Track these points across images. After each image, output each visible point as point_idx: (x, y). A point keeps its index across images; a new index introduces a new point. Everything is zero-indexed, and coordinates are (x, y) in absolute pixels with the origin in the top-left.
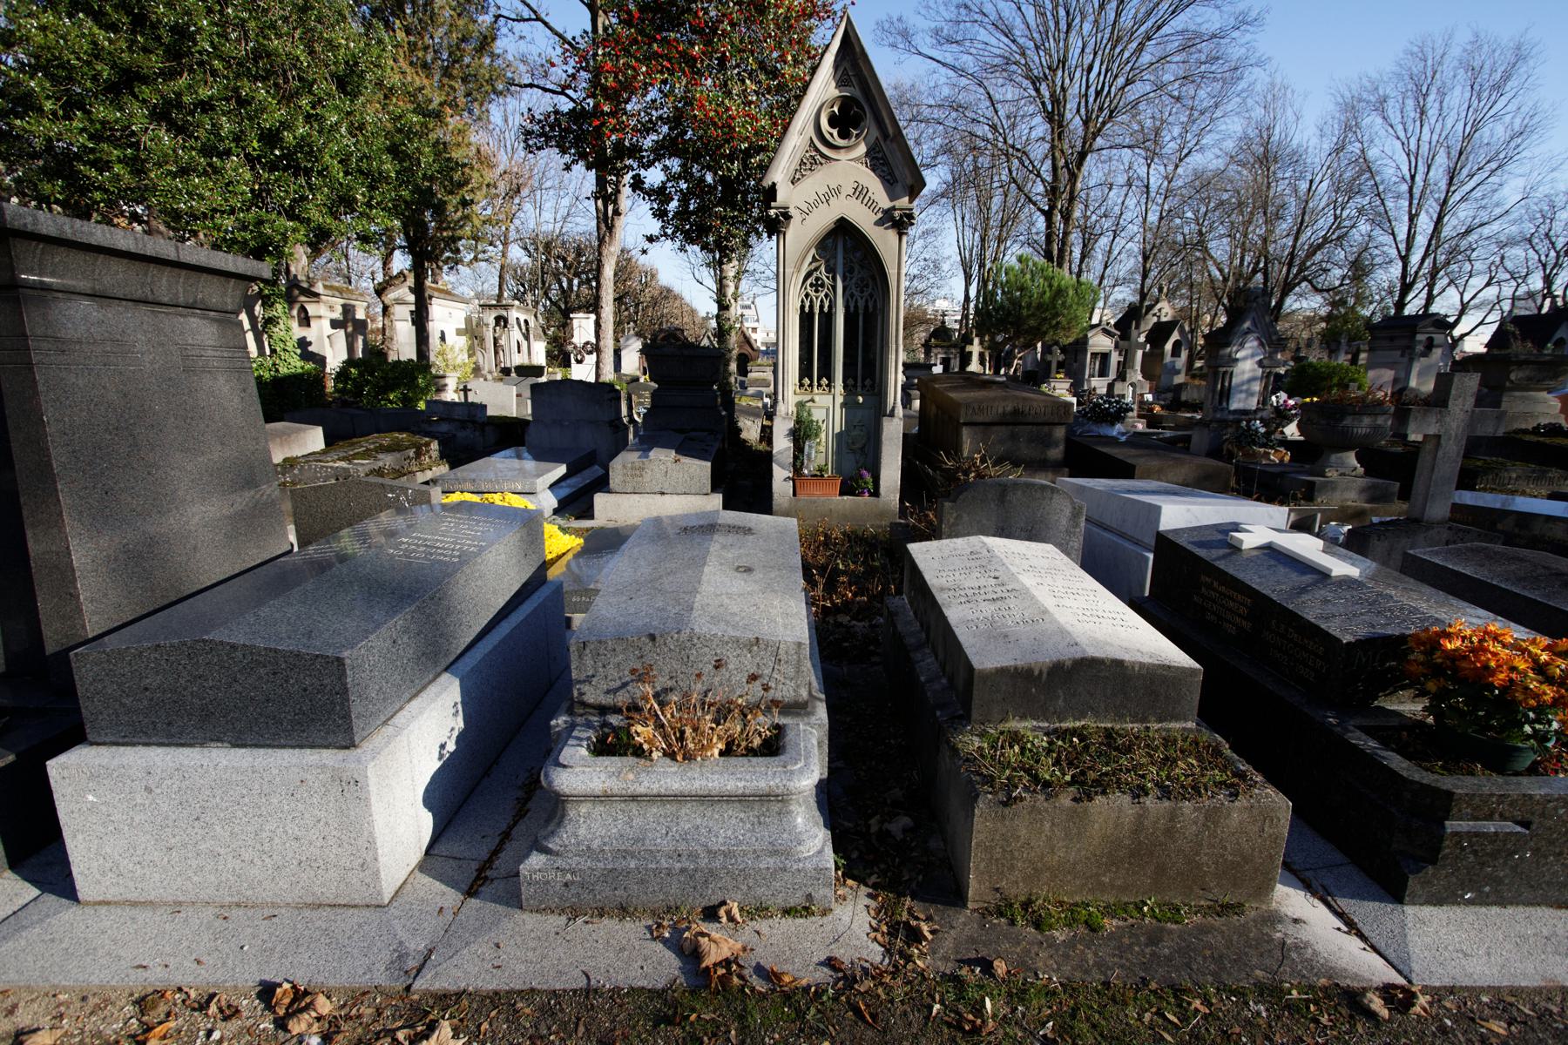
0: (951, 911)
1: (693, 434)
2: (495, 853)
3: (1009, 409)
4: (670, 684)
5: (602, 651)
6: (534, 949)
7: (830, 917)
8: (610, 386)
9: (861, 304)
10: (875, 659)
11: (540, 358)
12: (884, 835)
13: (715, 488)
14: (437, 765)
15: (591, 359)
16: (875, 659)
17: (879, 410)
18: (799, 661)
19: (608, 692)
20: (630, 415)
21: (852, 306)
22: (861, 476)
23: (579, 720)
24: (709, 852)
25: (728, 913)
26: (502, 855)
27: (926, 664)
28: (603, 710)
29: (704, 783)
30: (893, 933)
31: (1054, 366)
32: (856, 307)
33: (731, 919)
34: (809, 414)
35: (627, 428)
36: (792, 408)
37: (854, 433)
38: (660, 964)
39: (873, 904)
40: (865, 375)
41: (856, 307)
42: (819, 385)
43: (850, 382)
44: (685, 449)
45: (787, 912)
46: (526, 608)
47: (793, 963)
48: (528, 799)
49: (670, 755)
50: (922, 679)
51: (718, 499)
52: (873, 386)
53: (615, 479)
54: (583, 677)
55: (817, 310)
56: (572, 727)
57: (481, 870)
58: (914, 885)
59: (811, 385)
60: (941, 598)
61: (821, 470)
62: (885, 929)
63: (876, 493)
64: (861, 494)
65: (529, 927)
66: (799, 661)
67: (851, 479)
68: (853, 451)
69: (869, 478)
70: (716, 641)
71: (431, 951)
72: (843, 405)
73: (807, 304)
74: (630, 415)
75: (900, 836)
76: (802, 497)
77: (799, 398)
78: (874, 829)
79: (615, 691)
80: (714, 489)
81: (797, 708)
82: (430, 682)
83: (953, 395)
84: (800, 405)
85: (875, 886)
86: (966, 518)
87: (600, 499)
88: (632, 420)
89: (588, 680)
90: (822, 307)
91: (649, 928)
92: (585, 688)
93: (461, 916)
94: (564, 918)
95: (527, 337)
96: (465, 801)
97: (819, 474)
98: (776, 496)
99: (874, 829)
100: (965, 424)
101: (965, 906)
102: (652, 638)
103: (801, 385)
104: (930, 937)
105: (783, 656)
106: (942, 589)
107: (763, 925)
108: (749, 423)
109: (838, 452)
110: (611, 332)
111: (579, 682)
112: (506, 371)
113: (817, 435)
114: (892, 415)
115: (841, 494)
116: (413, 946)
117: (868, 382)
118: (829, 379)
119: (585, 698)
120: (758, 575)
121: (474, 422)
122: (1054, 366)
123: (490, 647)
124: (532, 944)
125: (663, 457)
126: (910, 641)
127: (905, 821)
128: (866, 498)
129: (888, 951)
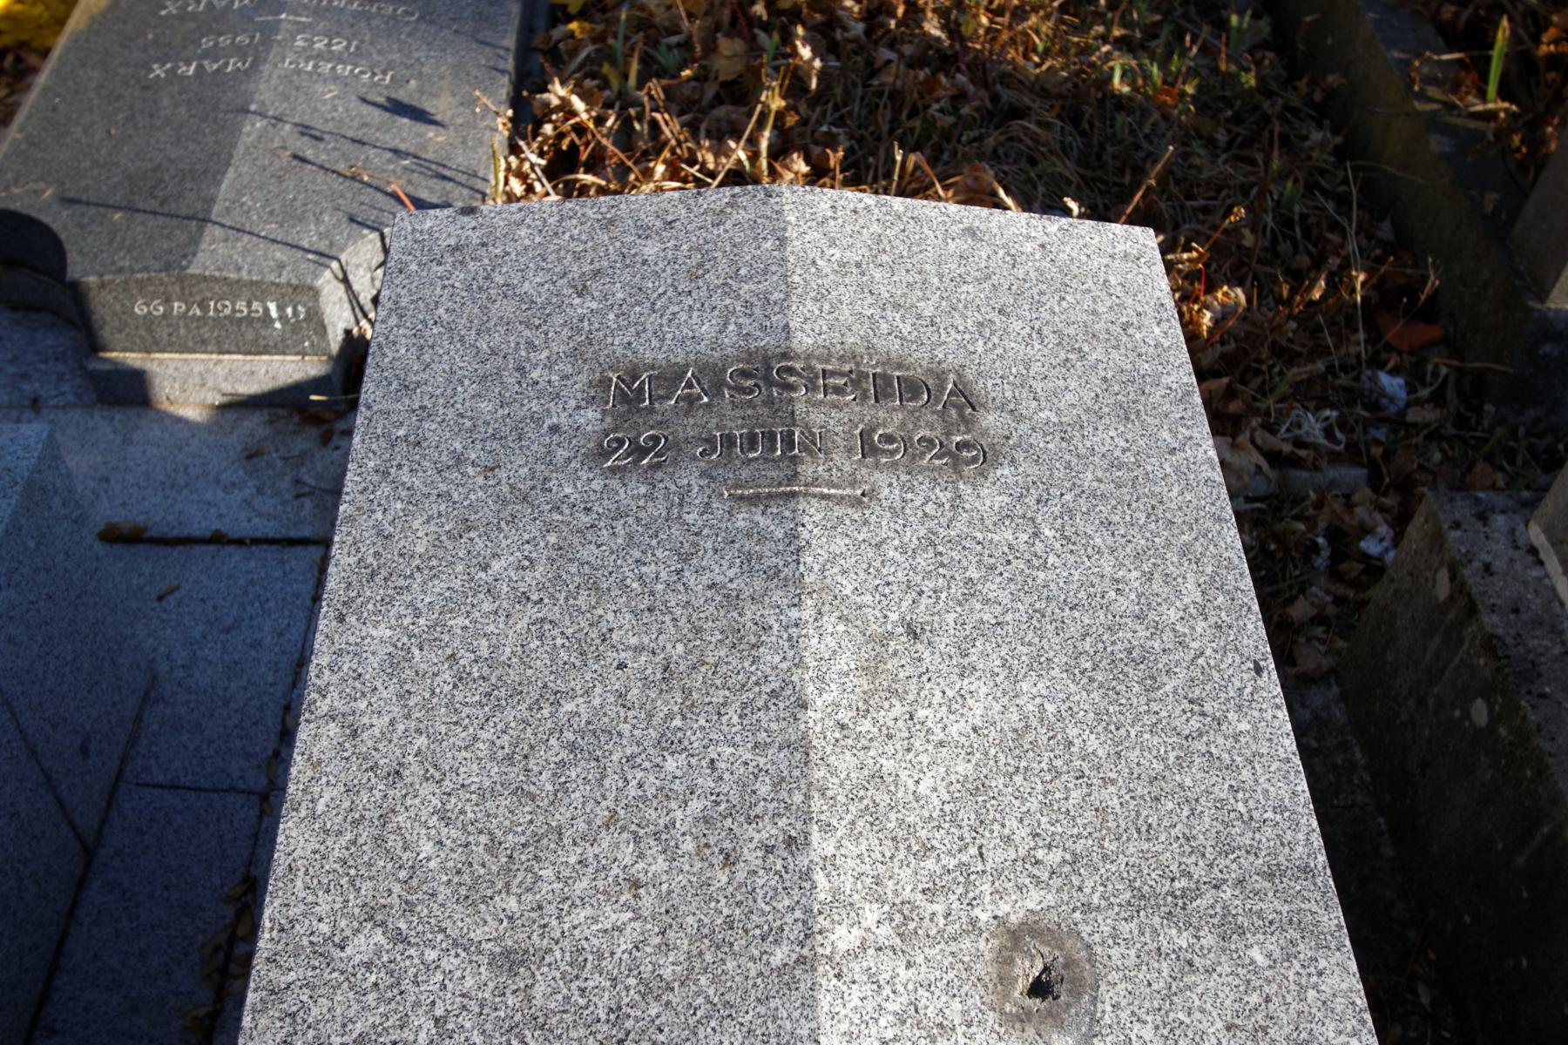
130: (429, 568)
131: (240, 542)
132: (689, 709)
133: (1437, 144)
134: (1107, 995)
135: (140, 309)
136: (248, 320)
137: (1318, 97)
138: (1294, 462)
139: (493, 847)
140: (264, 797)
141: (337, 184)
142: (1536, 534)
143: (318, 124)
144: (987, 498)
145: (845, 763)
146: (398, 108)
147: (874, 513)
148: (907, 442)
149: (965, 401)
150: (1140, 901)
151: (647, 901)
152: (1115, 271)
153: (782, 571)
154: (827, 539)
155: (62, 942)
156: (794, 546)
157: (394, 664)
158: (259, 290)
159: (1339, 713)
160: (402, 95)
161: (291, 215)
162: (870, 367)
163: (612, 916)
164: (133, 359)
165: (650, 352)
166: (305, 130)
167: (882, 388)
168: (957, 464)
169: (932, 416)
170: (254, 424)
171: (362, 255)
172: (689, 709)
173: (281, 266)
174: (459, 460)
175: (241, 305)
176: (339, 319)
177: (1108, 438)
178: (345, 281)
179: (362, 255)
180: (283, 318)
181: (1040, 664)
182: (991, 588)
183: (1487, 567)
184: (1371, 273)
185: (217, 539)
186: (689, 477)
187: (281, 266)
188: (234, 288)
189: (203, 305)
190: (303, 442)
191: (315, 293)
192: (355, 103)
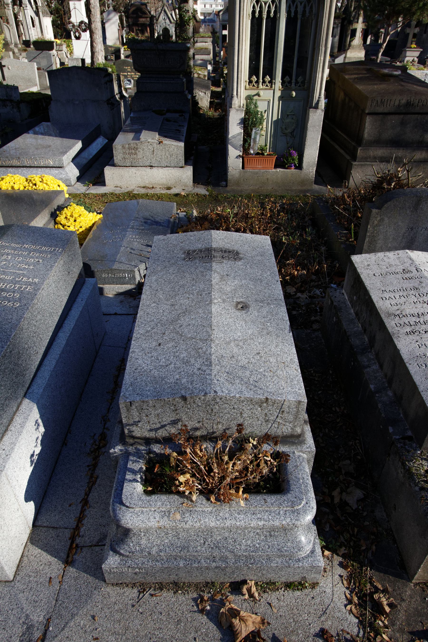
0: (399, 583)
1: (169, 115)
2: (80, 520)
3: (404, 101)
4: (197, 425)
5: (144, 407)
6: (119, 621)
7: (318, 589)
8: (103, 71)
9: (300, 9)
10: (315, 326)
11: (49, 35)
12: (344, 504)
13: (187, 162)
14: (29, 469)
15: (86, 35)
16: (315, 326)
17: (307, 103)
18: (298, 411)
19: (151, 430)
20: (120, 92)
21: (293, 10)
22: (291, 155)
23: (131, 449)
24: (235, 556)
25: (249, 590)
26: (85, 522)
27: (373, 372)
28: (148, 441)
29: (233, 522)
30: (361, 605)
31: (411, 36)
32: (296, 12)
33: (251, 596)
34: (256, 107)
35: (119, 104)
36: (243, 102)
37: (288, 121)
38: (207, 635)
39: (344, 573)
40: (299, 74)
41: (296, 12)
42: (264, 82)
43: (287, 79)
44: (166, 133)
45: (289, 585)
46: (75, 313)
47: (298, 635)
48: (95, 466)
49: (206, 493)
50: (372, 387)
51: (189, 171)
52: (303, 82)
53: (118, 153)
54: (131, 422)
55: (265, 16)
56: (126, 455)
57: (73, 539)
58: (370, 555)
59: (257, 82)
60: (391, 324)
61: (262, 149)
62: (355, 599)
63: (300, 167)
64: (289, 167)
65: (113, 599)
66: (298, 411)
67: (283, 156)
68: (286, 135)
69: (296, 156)
70: (234, 400)
71: (48, 620)
72: (280, 98)
73: (258, 10)
74: (120, 92)
75: (355, 507)
76: (248, 170)
77: (293, 168)
78: (337, 500)
79: (156, 430)
80: (187, 162)
81: (295, 439)
82: (15, 413)
83: (360, 87)
84: (249, 98)
85: (344, 556)
86: (386, 220)
87: (108, 171)
88: (122, 97)
89: (136, 424)
90: (269, 12)
91: (195, 600)
92: (134, 428)
93: (65, 586)
94: (135, 590)
95: (37, 13)
96: (50, 479)
97: (260, 153)
98: (230, 169)
99: (337, 500)
100: (369, 114)
101: (410, 579)
102: (184, 398)
103: (250, 82)
104: (387, 609)
105: (286, 409)
106: (389, 315)
107: (272, 597)
108: (202, 94)
109: (275, 136)
110: (98, 13)
111: (129, 425)
112: (27, 43)
113: (261, 123)
114: (316, 107)
115: (276, 167)
116: (36, 618)
117: (300, 79)
118: (271, 77)
119: (134, 434)
120: (253, 312)
121: (11, 101)
122: (411, 36)
123: (54, 362)
124: (117, 616)
125: (150, 138)
126: (355, 342)
127: (359, 493)
128: (293, 170)
129: (361, 623)
130: (160, 271)
131: (120, 315)
132: (196, 282)
133: (343, 246)
134: (250, 309)
135: (103, 276)
136: (122, 277)
137: (323, 242)
138: (315, 298)
139: (170, 296)
140: (125, 348)
141: (138, 256)
142: (343, 291)
143: (134, 248)
144: (240, 263)
145: (217, 286)
146: (148, 246)
147: (223, 264)
148: (228, 257)
149: (237, 253)
150: (256, 301)
151: (190, 299)
152: (264, 241)
153: (210, 269)
154: (215, 266)
155: (93, 365)
156: (211, 266)
157: (156, 281)
158: (124, 271)
159: (320, 335)
160: (149, 244)
161: (130, 260)
162: (224, 249)
163: (185, 301)
164: (101, 286)
165: (191, 248)
166: (132, 249)
167: (225, 252)
168: (235, 259)
169: (233, 255)
170: (122, 297)
171: (142, 266)
172: (196, 282)
173: (128, 268)
174: (164, 261)
175: (121, 274)
176: (138, 278)
177: (259, 258)
178: (139, 271)
179: (142, 266)
180: (128, 277)
181: (245, 279)
182: (239, 272)
183: (335, 297)
184: (327, 265)
185: (116, 314)
186: (197, 261)
187: (128, 268)
188: (120, 271)
189: (114, 275)
190: (131, 300)
191: (134, 272)
192: (140, 245)
